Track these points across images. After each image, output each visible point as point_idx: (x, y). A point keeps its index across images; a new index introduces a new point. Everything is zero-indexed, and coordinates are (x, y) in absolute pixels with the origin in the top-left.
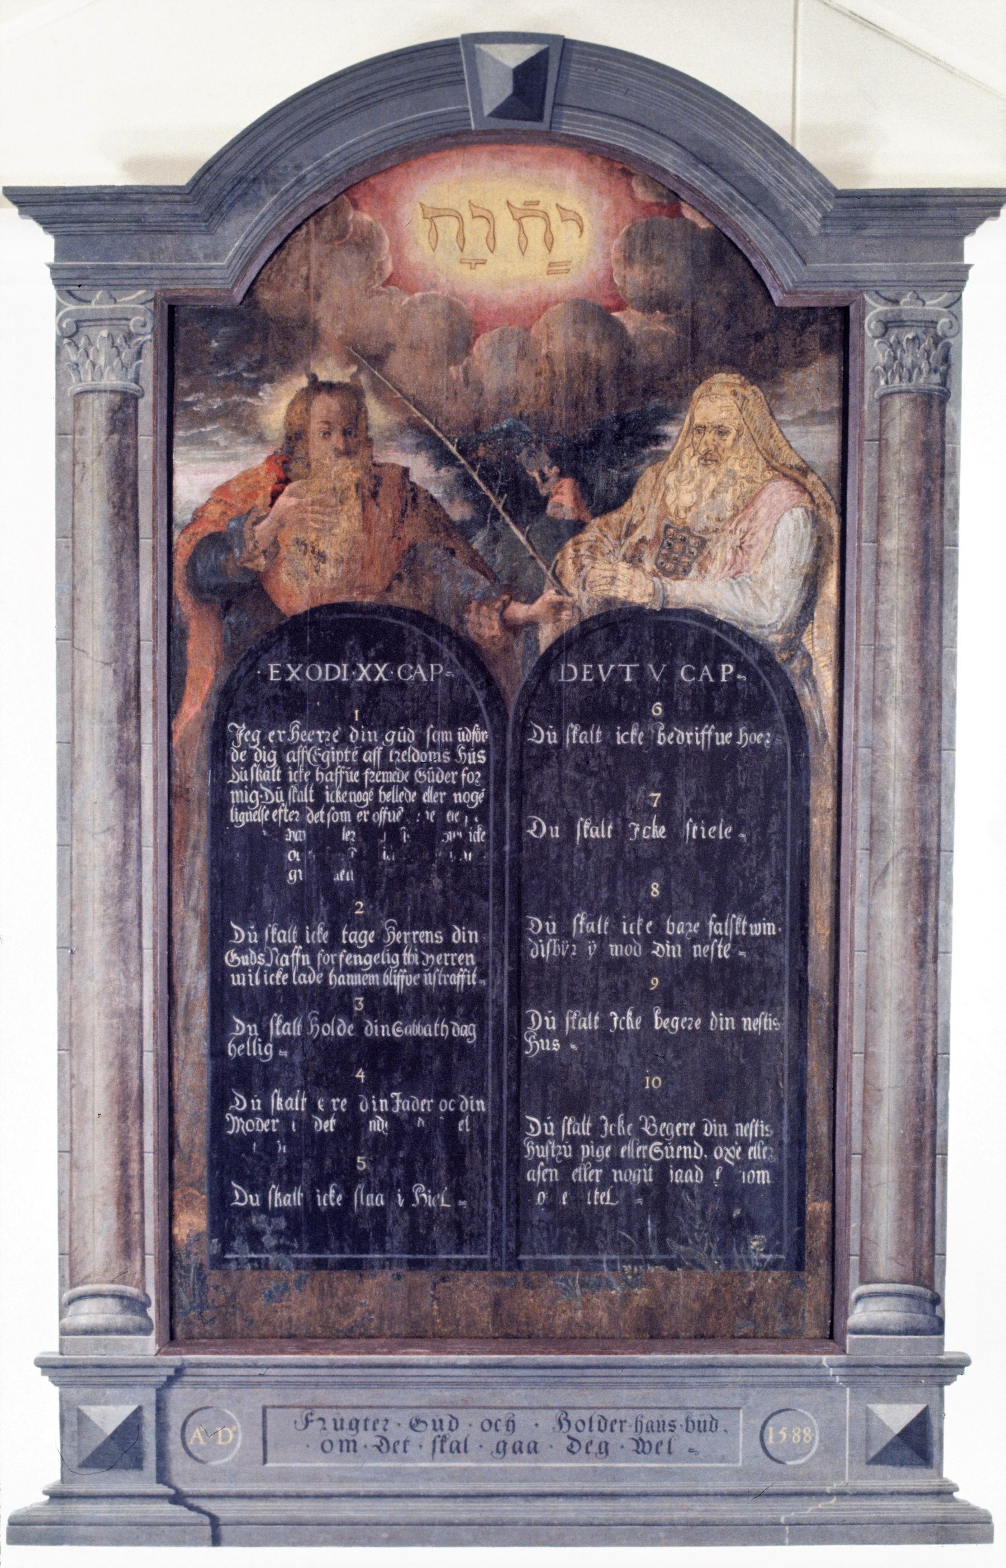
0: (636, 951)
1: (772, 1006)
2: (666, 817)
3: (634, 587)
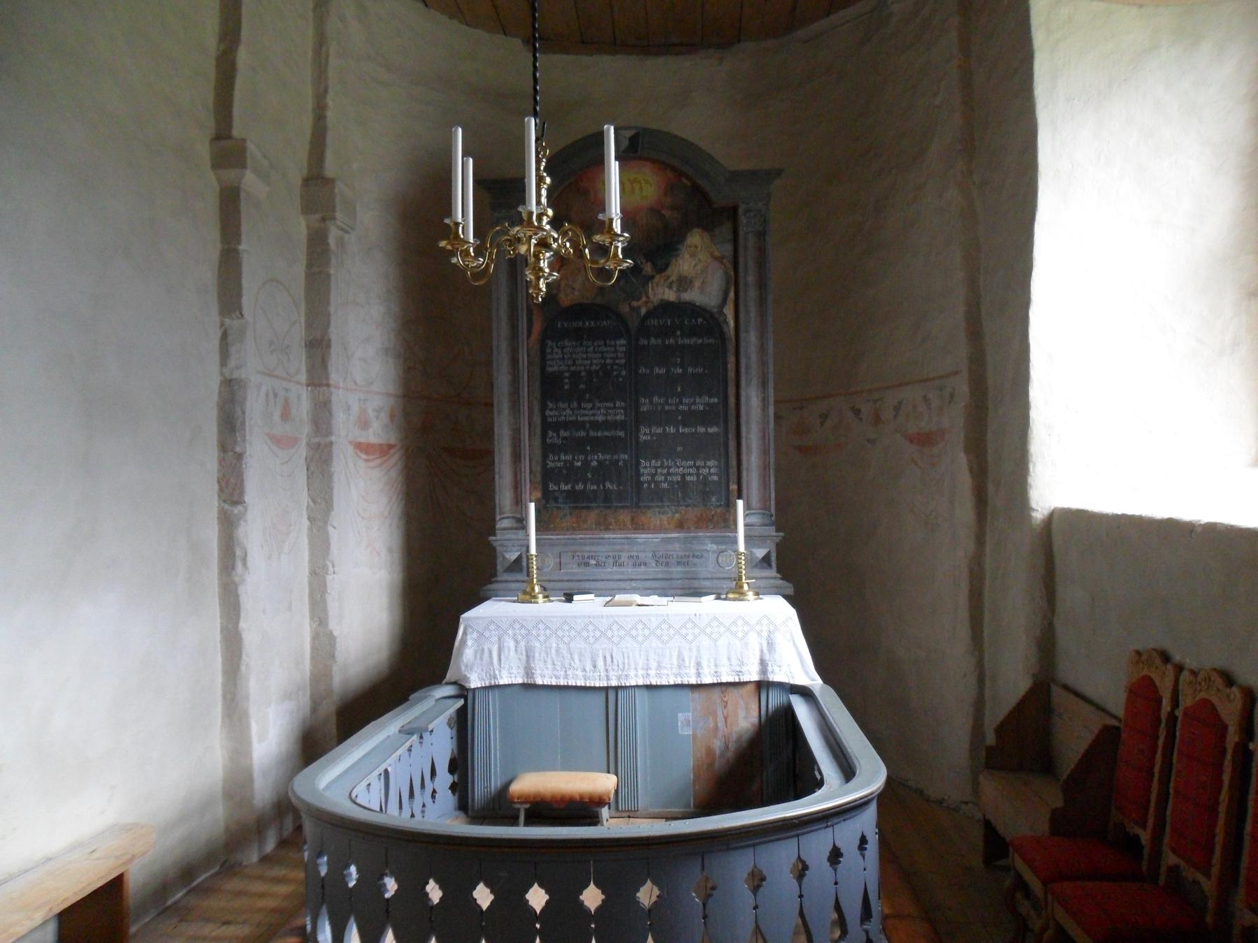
0: (673, 408)
1: (717, 424)
2: (682, 366)
3: (670, 295)
